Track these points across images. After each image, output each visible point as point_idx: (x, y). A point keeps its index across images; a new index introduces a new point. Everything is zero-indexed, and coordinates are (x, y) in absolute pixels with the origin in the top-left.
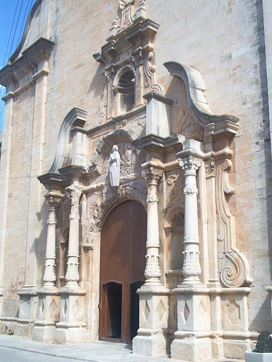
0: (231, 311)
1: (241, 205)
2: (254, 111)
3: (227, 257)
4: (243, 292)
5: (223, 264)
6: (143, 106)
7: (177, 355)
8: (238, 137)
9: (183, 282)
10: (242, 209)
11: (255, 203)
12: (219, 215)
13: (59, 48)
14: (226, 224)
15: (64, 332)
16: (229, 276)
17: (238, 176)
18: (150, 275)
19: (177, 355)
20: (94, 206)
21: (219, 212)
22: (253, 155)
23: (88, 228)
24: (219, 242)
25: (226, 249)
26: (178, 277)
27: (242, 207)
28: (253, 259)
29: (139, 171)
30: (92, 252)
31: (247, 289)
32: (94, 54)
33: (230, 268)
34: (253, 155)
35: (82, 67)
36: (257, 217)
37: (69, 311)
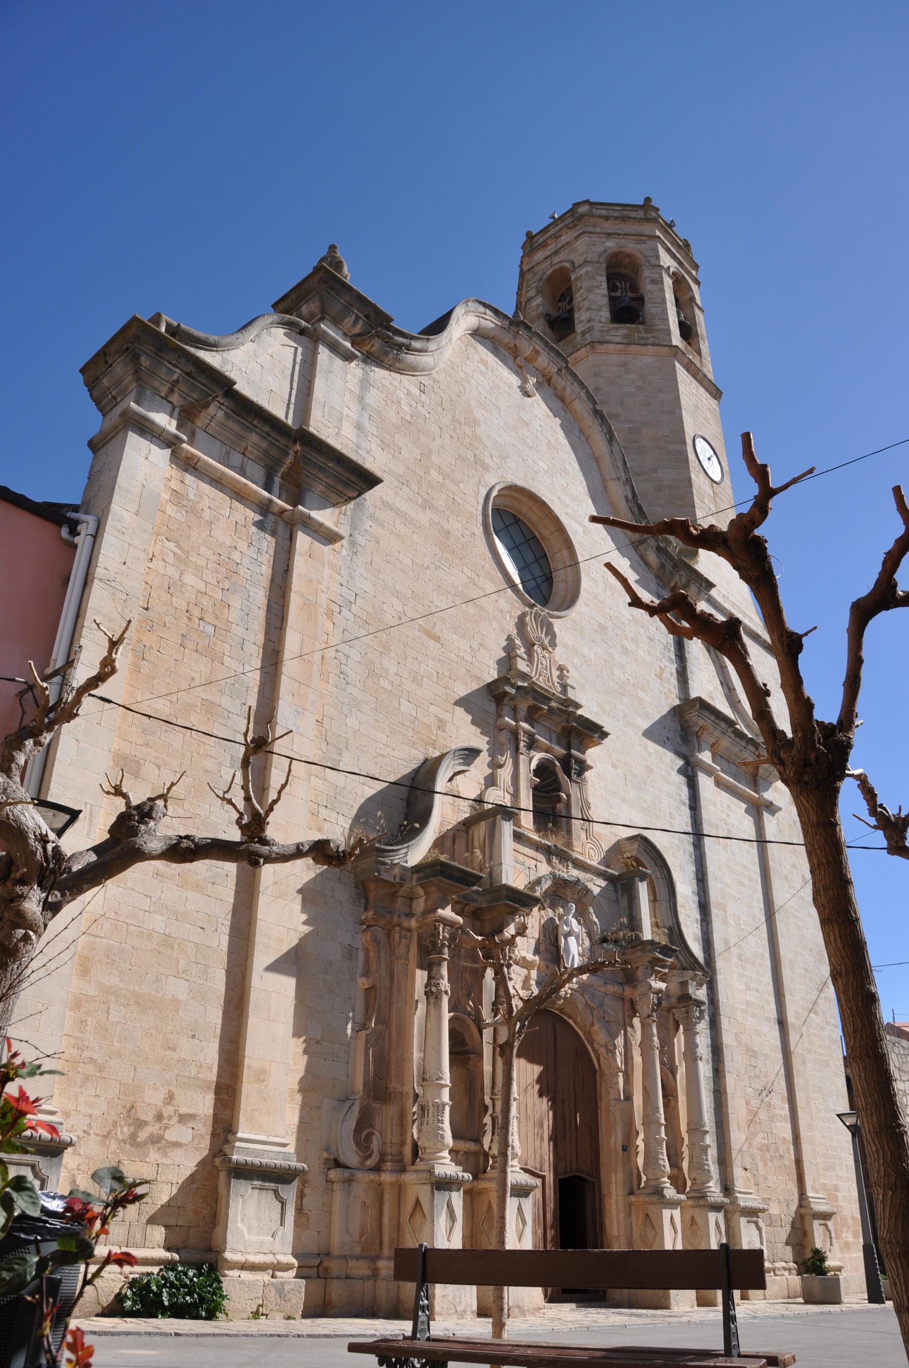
35: (439, 646)
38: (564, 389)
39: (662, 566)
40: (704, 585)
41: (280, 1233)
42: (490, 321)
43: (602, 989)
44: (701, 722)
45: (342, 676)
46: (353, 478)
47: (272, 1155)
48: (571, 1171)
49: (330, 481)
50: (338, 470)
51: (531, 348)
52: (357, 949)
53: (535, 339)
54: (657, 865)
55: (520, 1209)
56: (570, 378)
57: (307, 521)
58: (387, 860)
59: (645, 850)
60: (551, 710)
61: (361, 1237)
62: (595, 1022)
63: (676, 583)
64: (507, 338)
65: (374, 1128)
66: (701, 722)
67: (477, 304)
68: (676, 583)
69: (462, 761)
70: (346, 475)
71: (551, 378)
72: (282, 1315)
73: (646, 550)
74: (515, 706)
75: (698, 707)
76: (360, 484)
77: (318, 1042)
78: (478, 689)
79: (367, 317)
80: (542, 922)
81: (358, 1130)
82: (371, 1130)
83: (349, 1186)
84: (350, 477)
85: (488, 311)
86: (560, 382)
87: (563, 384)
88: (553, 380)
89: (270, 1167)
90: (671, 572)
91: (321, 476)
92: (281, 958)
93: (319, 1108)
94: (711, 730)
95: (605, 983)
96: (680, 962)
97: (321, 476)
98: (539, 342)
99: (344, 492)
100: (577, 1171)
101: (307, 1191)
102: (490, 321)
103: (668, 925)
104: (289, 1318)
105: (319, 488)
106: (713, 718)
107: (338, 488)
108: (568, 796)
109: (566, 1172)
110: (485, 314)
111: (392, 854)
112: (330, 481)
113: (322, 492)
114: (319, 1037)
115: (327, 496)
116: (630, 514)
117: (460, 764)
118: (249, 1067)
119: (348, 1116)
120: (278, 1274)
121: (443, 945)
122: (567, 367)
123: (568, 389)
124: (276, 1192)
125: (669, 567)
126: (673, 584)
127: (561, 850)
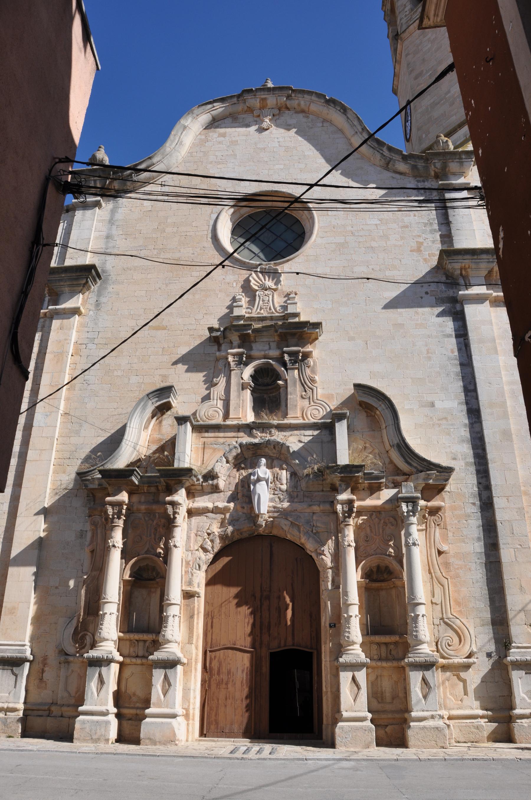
0: (453, 686)
1: (457, 567)
2: (468, 470)
3: (446, 623)
4: (426, 663)
5: (441, 631)
6: (304, 422)
7: (419, 743)
8: (449, 492)
9: (95, 647)
10: (458, 571)
11: (473, 566)
12: (433, 575)
13: (301, 314)
14: (443, 586)
15: (170, 724)
16: (449, 646)
17: (450, 534)
18: (106, 638)
19: (419, 743)
20: (206, 534)
21: (432, 571)
22: (469, 516)
23: (191, 563)
24: (434, 605)
25: (444, 615)
26: (138, 643)
27: (458, 569)
28: (475, 627)
29: (302, 501)
30: (198, 601)
31: (471, 660)
32: (211, 326)
33: (452, 636)
34: (469, 516)
35: (166, 331)
36: (477, 582)
37: (175, 690)
38: (299, 105)
39: (414, 168)
40: (464, 157)
41: (13, 692)
42: (220, 107)
43: (308, 510)
44: (457, 266)
45: (84, 382)
46: (78, 274)
47: (11, 651)
48: (285, 646)
49: (68, 283)
50: (69, 275)
51: (258, 100)
52: (86, 531)
53: (258, 93)
54: (379, 401)
55: (354, 679)
56: (300, 95)
57: (56, 311)
58: (89, 478)
59: (365, 393)
60: (255, 331)
61: (76, 693)
62: (301, 536)
63: (434, 171)
64: (240, 107)
65: (88, 632)
66: (457, 266)
67: (204, 107)
68: (434, 171)
69: (157, 399)
70: (74, 275)
71: (286, 105)
72: (5, 735)
73: (394, 165)
74: (231, 341)
75: (445, 257)
76: (84, 274)
77: (57, 588)
78: (201, 343)
79: (99, 177)
80: (241, 477)
81: (76, 632)
82: (85, 632)
83: (69, 665)
84: (77, 274)
85: (215, 104)
86: (293, 103)
87: (296, 102)
88: (288, 106)
89: (5, 657)
90: (424, 167)
91: (62, 284)
92: (27, 547)
93: (56, 623)
94: (473, 266)
95: (310, 506)
96: (415, 467)
97: (62, 284)
98: (262, 93)
99: (79, 283)
100: (293, 645)
101: (46, 669)
102: (220, 107)
103: (396, 442)
104: (10, 737)
105: (67, 289)
106: (468, 257)
107: (75, 283)
108: (286, 381)
109: (279, 647)
110: (214, 107)
111: (90, 473)
112: (68, 283)
113: (70, 290)
114: (57, 585)
115: (73, 290)
116: (372, 150)
117: (157, 401)
118: (6, 607)
119: (69, 626)
120: (8, 713)
121: (113, 518)
122: (293, 91)
123: (302, 103)
124: (12, 670)
125: (420, 164)
126: (433, 173)
127: (259, 423)
